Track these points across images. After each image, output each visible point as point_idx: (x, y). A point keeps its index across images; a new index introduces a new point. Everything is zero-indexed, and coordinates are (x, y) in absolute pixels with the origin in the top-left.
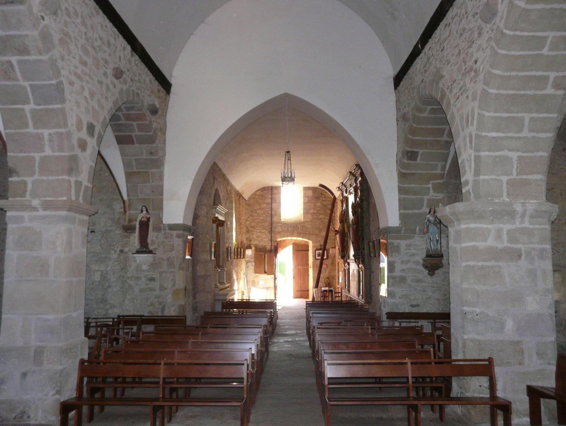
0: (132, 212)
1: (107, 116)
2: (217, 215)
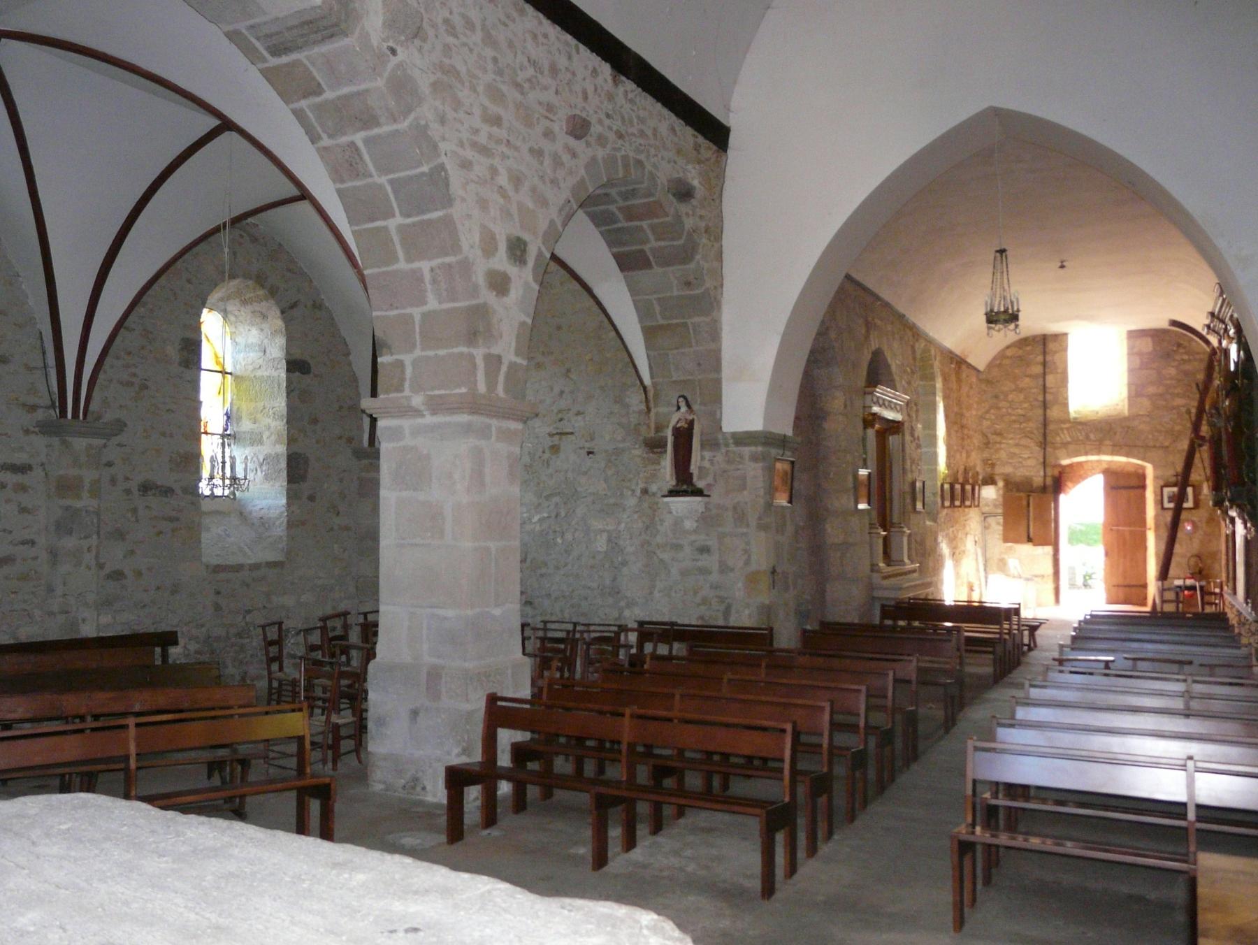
0: (663, 410)
1: (556, 219)
2: (876, 409)
